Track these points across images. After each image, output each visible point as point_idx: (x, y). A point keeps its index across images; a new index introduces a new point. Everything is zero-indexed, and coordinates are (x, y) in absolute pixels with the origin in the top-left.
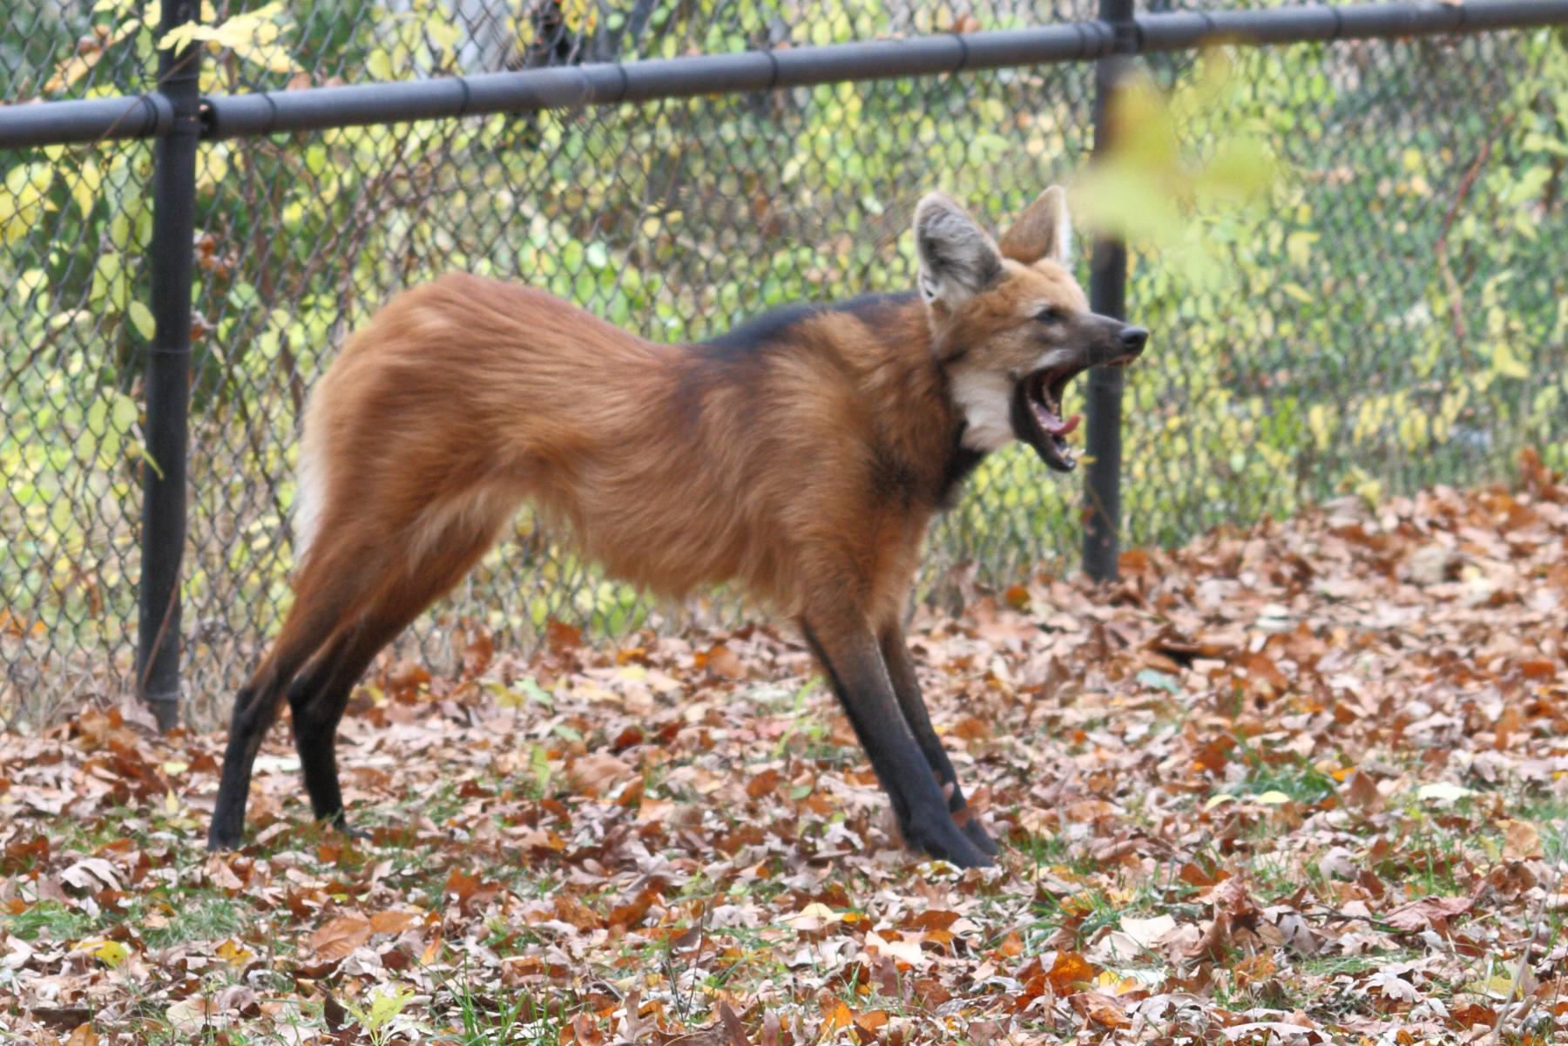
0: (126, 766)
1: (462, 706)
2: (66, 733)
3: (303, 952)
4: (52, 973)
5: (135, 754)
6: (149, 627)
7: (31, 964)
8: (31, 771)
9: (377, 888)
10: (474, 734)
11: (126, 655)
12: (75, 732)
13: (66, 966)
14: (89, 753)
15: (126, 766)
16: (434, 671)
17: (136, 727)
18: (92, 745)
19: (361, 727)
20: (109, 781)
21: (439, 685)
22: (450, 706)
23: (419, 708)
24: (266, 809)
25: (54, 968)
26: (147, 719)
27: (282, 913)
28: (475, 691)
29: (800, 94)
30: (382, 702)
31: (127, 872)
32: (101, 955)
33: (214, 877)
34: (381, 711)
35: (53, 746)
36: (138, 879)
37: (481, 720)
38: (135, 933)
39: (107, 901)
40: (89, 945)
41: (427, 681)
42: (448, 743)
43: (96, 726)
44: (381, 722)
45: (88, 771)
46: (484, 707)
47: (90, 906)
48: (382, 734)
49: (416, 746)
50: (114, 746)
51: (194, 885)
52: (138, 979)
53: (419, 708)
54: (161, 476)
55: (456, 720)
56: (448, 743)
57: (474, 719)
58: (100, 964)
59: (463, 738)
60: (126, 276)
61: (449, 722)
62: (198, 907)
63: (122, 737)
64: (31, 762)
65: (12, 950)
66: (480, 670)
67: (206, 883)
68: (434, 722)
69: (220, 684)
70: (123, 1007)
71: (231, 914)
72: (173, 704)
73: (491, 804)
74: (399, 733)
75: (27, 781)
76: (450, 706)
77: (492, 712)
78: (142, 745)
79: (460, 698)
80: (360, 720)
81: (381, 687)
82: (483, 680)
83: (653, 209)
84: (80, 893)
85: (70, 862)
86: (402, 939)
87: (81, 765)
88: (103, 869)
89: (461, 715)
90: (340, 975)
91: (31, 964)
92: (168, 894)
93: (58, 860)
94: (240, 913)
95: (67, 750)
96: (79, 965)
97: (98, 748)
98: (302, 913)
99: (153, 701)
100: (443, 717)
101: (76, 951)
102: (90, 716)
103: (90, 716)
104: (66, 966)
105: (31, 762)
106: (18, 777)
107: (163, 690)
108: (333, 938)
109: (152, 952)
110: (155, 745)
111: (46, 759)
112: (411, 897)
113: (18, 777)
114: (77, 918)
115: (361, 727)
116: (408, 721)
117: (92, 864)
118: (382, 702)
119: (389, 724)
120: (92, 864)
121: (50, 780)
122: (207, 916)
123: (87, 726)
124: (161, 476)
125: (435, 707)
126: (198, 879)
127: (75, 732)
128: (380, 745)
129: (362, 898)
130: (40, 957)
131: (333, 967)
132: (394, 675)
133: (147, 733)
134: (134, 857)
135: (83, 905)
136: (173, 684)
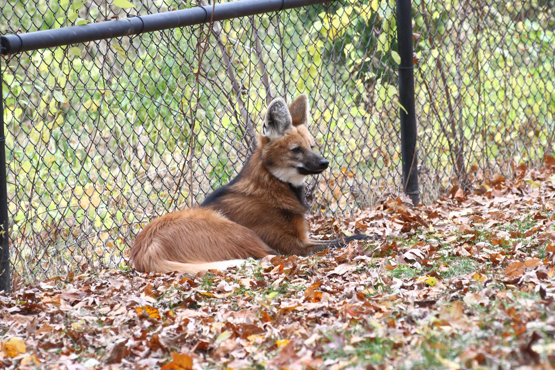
0: (405, 218)
1: (519, 189)
2: (382, 208)
3: (502, 276)
4: (411, 289)
5: (408, 214)
6: (406, 168)
7: (403, 287)
8: (373, 222)
9: (519, 253)
10: (525, 198)
11: (398, 180)
12: (385, 208)
13: (416, 287)
14: (391, 214)
15: (405, 218)
16: (506, 177)
17: (407, 204)
18: (392, 212)
19: (484, 199)
20: (401, 224)
21: (508, 182)
22: (515, 189)
23: (503, 191)
24: (465, 228)
25: (412, 288)
26: (409, 201)
27: (487, 263)
28: (523, 183)
29: (218, 26)
30: (489, 189)
31: (426, 253)
32: (427, 282)
33: (460, 252)
34: (490, 192)
35: (379, 213)
36: (431, 255)
37: (527, 193)
38: (439, 274)
39: (424, 263)
40: (421, 279)
41: (504, 181)
42: (516, 202)
43: (392, 205)
44: (490, 197)
45: (393, 221)
46: (527, 189)
47: (417, 265)
48: (492, 201)
49: (505, 204)
50: (400, 211)
51: (454, 255)
52: (443, 289)
53: (503, 191)
54: (407, 113)
55: (517, 194)
56: (516, 202)
57: (524, 194)
58: (427, 286)
59: (521, 200)
60: (389, 42)
61: (515, 195)
62: (457, 263)
63: (402, 208)
64: (372, 219)
65: (396, 283)
66: (523, 176)
67: (458, 254)
68: (509, 195)
69: (432, 187)
70: (446, 299)
71: (470, 265)
72: (417, 195)
73: (547, 221)
74: (497, 200)
75: (372, 226)
76: (515, 189)
77: (530, 190)
78: (410, 210)
79: (518, 186)
80: (483, 197)
81: (487, 184)
82: (525, 179)
83: (541, 9)
84: (412, 261)
85: (405, 251)
86: (539, 269)
87: (390, 219)
88: (418, 252)
89: (519, 192)
90: (522, 282)
91: (403, 287)
92: (444, 259)
93: (401, 250)
94: (473, 264)
95: (385, 214)
96: (420, 286)
97: (394, 213)
98: (496, 263)
99: (410, 195)
100: (513, 194)
101: (418, 281)
102: (390, 201)
103: (390, 201)
104: (416, 287)
105: (372, 219)
106: (369, 224)
107: (413, 191)
108: (512, 270)
109: (447, 280)
110: (414, 210)
111: (378, 217)
112: (533, 255)
113: (369, 224)
114: (414, 270)
115: (484, 199)
116: (500, 196)
117: (414, 251)
118: (489, 189)
119: (494, 197)
120: (414, 251)
121: (381, 225)
122: (462, 266)
123: (389, 205)
124: (407, 113)
125: (509, 190)
126: (455, 253)
127: (385, 208)
128: (492, 205)
129: (515, 256)
130: (406, 284)
131: (518, 280)
132: (492, 180)
133: (410, 206)
134: (427, 247)
135: (415, 265)
136: (416, 188)
